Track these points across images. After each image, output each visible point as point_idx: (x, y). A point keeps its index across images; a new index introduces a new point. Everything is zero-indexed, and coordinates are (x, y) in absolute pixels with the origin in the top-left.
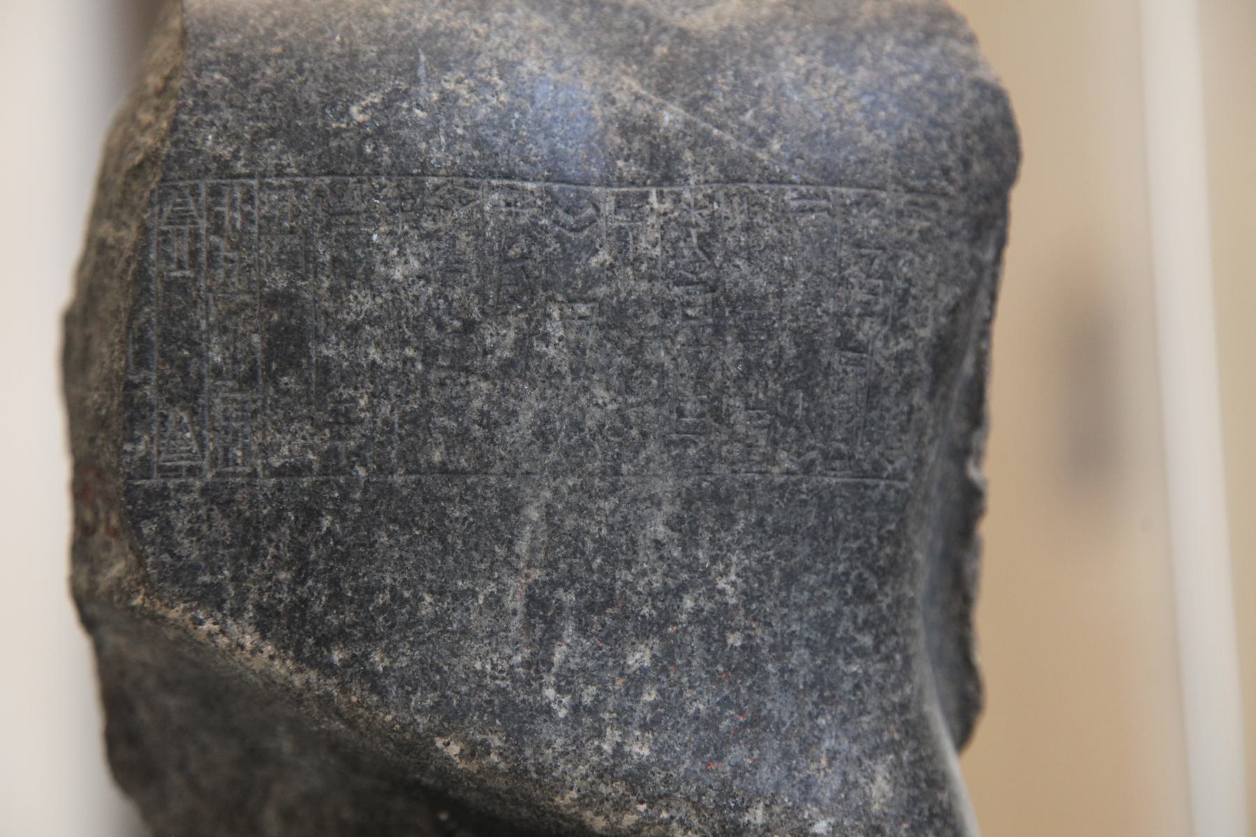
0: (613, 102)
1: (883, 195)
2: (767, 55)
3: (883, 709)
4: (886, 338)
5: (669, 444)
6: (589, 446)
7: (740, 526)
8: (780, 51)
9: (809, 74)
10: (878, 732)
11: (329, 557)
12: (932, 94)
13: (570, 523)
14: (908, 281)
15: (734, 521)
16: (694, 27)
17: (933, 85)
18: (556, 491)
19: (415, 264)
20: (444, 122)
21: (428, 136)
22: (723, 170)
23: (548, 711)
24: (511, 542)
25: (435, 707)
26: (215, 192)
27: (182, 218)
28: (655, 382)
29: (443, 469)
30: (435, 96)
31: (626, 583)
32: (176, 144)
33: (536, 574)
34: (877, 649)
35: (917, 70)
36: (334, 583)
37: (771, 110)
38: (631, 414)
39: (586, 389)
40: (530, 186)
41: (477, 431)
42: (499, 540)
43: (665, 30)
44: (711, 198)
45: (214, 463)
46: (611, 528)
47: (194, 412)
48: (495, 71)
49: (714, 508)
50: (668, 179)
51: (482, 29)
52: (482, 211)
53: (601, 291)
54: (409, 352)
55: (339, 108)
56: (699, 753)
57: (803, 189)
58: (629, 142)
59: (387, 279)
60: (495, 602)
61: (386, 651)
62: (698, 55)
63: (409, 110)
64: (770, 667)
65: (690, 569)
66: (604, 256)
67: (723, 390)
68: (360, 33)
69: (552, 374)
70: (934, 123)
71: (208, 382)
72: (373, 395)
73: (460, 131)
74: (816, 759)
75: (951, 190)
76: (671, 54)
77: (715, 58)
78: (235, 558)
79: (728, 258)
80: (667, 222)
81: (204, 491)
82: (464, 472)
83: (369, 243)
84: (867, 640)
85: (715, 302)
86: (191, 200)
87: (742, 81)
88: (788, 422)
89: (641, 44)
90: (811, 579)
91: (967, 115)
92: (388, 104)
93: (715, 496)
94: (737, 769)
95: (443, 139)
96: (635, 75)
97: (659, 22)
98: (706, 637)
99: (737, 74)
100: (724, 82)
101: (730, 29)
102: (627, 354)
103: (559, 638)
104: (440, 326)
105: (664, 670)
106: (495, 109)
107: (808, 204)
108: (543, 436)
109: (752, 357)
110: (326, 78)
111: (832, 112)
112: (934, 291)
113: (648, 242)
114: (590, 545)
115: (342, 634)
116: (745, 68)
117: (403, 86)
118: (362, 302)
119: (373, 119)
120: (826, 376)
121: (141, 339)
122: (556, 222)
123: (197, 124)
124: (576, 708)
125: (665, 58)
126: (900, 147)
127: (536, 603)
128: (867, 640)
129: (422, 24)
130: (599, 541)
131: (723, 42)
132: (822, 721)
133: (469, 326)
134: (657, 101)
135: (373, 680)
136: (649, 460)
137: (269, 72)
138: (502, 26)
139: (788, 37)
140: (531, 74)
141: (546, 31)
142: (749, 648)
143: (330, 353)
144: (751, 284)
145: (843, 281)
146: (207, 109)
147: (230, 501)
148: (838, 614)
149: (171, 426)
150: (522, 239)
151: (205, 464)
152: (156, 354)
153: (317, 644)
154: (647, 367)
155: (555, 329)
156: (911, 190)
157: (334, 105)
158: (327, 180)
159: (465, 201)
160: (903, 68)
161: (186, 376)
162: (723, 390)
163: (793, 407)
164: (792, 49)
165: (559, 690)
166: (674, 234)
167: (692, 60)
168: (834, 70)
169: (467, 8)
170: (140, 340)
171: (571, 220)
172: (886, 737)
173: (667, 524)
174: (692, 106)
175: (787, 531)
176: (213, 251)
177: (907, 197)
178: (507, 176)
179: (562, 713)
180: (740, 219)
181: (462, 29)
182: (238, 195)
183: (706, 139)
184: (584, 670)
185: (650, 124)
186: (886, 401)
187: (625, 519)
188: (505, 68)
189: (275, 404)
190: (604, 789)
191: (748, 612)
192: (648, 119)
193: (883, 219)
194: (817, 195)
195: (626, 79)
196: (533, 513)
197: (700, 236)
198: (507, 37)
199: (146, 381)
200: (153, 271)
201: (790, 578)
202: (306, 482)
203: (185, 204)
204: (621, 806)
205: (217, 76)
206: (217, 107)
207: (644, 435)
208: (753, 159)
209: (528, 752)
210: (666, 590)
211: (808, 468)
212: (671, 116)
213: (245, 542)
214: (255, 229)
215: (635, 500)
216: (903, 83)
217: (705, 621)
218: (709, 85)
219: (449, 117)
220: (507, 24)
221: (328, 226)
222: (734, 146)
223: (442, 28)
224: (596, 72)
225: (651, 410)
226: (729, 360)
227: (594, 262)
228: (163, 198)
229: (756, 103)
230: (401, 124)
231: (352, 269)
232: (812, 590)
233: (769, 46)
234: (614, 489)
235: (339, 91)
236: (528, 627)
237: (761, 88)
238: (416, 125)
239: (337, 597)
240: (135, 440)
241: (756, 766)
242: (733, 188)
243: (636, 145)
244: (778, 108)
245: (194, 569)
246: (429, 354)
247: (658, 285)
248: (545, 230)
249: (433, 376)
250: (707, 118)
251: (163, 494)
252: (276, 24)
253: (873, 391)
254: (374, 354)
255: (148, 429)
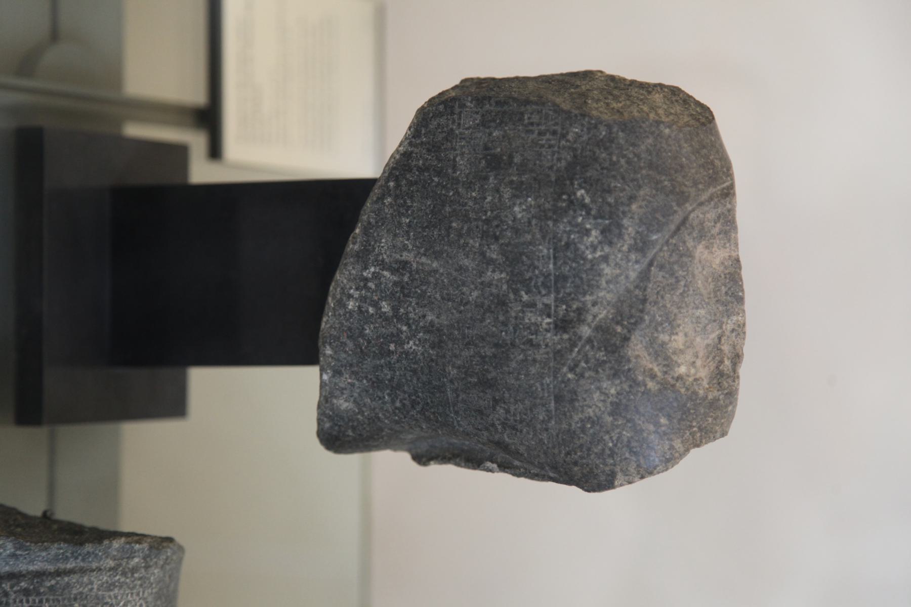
0: (593, 305)
1: (553, 423)
2: (615, 375)
3: (374, 409)
4: (499, 420)
5: (458, 322)
6: (457, 288)
7: (431, 352)
8: (617, 382)
9: (606, 394)
10: (365, 405)
11: (424, 181)
12: (603, 450)
13: (432, 279)
14: (521, 432)
15: (433, 348)
16: (631, 345)
17: (608, 452)
18: (442, 274)
19: (519, 216)
20: (576, 230)
21: (570, 223)
22: (559, 351)
23: (366, 268)
24: (425, 255)
25: (369, 223)
26: (554, 133)
27: (546, 118)
28: (479, 317)
29: (450, 227)
30: (588, 226)
31: (411, 302)
32: (576, 116)
33: (415, 265)
34: (396, 408)
35: (615, 445)
36: (416, 183)
37: (587, 375)
38: (468, 307)
39: (476, 288)
40: (551, 266)
41: (462, 241)
42: (426, 250)
43: (629, 331)
44: (547, 346)
45: (461, 134)
46: (430, 297)
47: (478, 125)
48: (602, 253)
49: (436, 340)
50: (556, 326)
51: (625, 248)
52: (539, 245)
53: (512, 296)
54: (489, 213)
55: (583, 185)
56: (350, 329)
57: (551, 386)
58: (574, 312)
59: (514, 204)
60: (405, 248)
61: (391, 204)
62: (615, 344)
63: (581, 215)
64: (383, 361)
65: (416, 329)
66: (525, 297)
67: (476, 346)
68: (621, 195)
69: (481, 274)
70: (589, 449)
71: (487, 131)
72: (475, 198)
73: (572, 236)
74: (350, 378)
75: (562, 455)
76: (616, 333)
77: (614, 352)
78: (429, 143)
79: (523, 350)
80: (538, 326)
81: (452, 130)
82: (449, 236)
83: (528, 197)
84: (398, 404)
85: (507, 344)
86: (553, 122)
87: (601, 364)
88: (466, 373)
89: (622, 320)
90: (415, 381)
91: (597, 466)
92: (584, 206)
93: (441, 341)
94: (344, 344)
95: (568, 229)
96: (607, 316)
97: (634, 330)
98: (392, 335)
99: (604, 362)
100: (601, 355)
101: (629, 361)
102: (489, 306)
103: (392, 274)
104: (497, 226)
105: (381, 317)
106: (583, 252)
107: (545, 386)
108: (461, 269)
109: (487, 359)
110: (598, 180)
111: (586, 403)
112: (522, 444)
113: (531, 317)
114: (424, 288)
115: (398, 186)
116: (608, 365)
117: (593, 212)
118: (507, 193)
119: (577, 199)
120: (483, 391)
121: (505, 103)
122: (537, 277)
123: (583, 125)
124: (366, 280)
125: (615, 331)
126: (574, 432)
127: (405, 264)
128: (398, 404)
129: (626, 222)
130: (425, 292)
131: (622, 357)
132: (365, 381)
133: (497, 238)
134: (593, 325)
135: (381, 198)
136: (452, 313)
137: (604, 155)
138: (627, 257)
139: (626, 387)
140: (603, 269)
141: (627, 277)
142: (390, 353)
143: (491, 180)
144: (512, 360)
145: (516, 402)
146: (589, 129)
147: (447, 140)
148: (405, 392)
149: (475, 116)
150: (529, 262)
151: (461, 130)
152: (499, 109)
153: (397, 176)
154: (484, 314)
155: (497, 276)
156: (557, 436)
157: (585, 182)
158: (553, 179)
159: (544, 237)
160: (614, 438)
161: (490, 121)
162: (476, 346)
163: (471, 376)
164: (619, 388)
165: (374, 273)
166: (533, 328)
167: (612, 342)
168: (608, 405)
169: (636, 243)
170: (505, 102)
171: (539, 284)
172: (364, 409)
173: (432, 321)
174: (589, 341)
175: (430, 371)
176: (532, 132)
177: (554, 434)
178: (555, 258)
179: (365, 274)
180: (538, 357)
181: (625, 241)
182: (553, 142)
183: (574, 345)
184: (381, 284)
185: (581, 321)
186: (479, 418)
187: (433, 303)
188: (605, 259)
189: (476, 158)
190: (338, 289)
191: (402, 353)
192: (584, 321)
193: (543, 421)
194: (549, 392)
195: (605, 312)
196: (435, 265)
197: (531, 340)
198: (622, 260)
199: (491, 105)
200: (528, 107)
201: (414, 371)
202: (450, 171)
203: (552, 119)
204: (334, 297)
205: (604, 133)
206: (589, 133)
207: (461, 312)
208: (564, 365)
209: (352, 260)
210: (408, 319)
211: (451, 381)
212: (585, 331)
213: (433, 146)
214: (537, 149)
215: (440, 307)
216: (607, 437)
217: (398, 335)
218: (599, 349)
219: (578, 232)
220: (629, 261)
221: (535, 179)
222: (569, 357)
223: (624, 231)
224: (609, 299)
225: (469, 315)
226: (486, 349)
227: (523, 293)
228: (555, 111)
229: (589, 369)
230: (575, 211)
231: (520, 190)
232: (411, 381)
233: (619, 378)
234: (443, 298)
235: (591, 185)
236: (397, 261)
237: (597, 372)
238: (574, 218)
239: (411, 184)
240: (471, 102)
241: (345, 352)
242: (551, 355)
243: (572, 314)
244: (588, 378)
245: (426, 126)
246: (487, 221)
247: (513, 321)
248: (533, 272)
249: (480, 223)
250: (583, 346)
251: (452, 113)
252: (629, 158)
253: (480, 412)
254: (489, 199)
255: (475, 106)
